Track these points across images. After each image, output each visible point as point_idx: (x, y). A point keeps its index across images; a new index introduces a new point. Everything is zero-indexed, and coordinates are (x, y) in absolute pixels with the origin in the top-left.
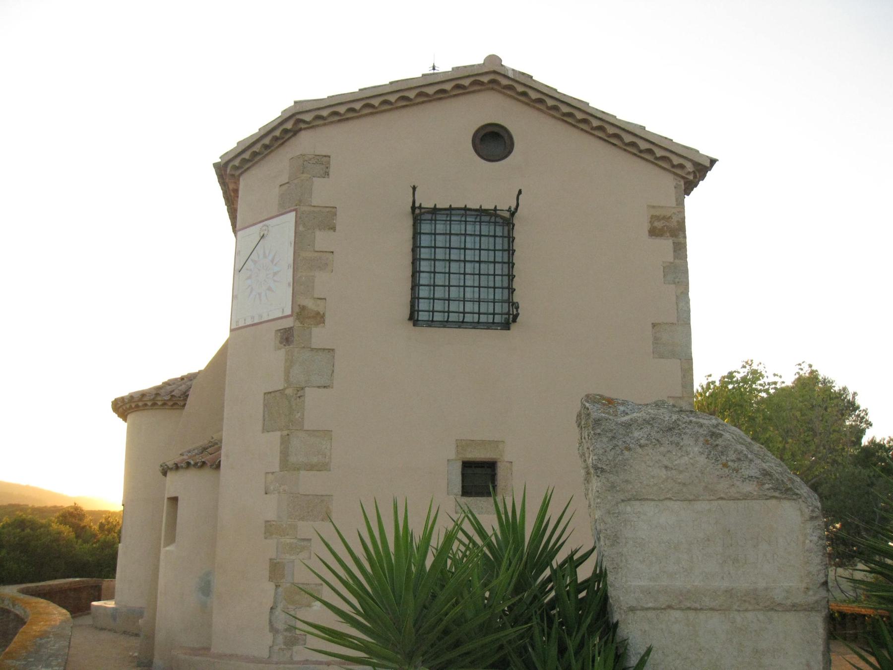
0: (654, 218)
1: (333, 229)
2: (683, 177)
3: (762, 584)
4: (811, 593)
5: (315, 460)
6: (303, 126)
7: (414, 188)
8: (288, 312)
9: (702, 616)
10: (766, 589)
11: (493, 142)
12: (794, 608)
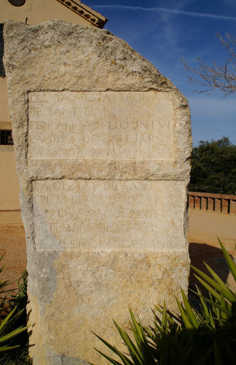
3: (139, 159)
4: (178, 165)
9: (90, 183)
10: (143, 163)
12: (165, 178)
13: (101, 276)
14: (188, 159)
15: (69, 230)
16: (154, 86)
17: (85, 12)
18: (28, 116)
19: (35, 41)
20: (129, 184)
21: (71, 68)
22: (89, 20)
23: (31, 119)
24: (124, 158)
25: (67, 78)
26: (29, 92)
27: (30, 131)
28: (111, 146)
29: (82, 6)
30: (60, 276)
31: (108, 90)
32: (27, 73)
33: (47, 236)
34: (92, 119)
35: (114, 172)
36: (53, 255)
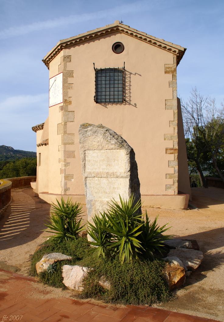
0: (166, 68)
1: (73, 77)
2: (176, 55)
3: (115, 171)
4: (126, 173)
5: (70, 142)
6: (63, 47)
7: (94, 64)
8: (62, 102)
9: (102, 179)
10: (116, 172)
11: (118, 48)
12: (122, 177)
13: (104, 208)
14: (129, 171)
15: (96, 193)
16: (119, 148)
17: (167, 47)
18: (85, 158)
19: (86, 135)
20: (112, 179)
21: (96, 143)
22: (172, 52)
23: (86, 159)
24: (111, 171)
25: (95, 146)
26: (85, 150)
27: (86, 163)
28: (108, 167)
29: (164, 45)
30: (93, 207)
31: (106, 149)
32: (85, 144)
33: (90, 195)
34: (102, 159)
35: (108, 175)
36: (91, 201)
